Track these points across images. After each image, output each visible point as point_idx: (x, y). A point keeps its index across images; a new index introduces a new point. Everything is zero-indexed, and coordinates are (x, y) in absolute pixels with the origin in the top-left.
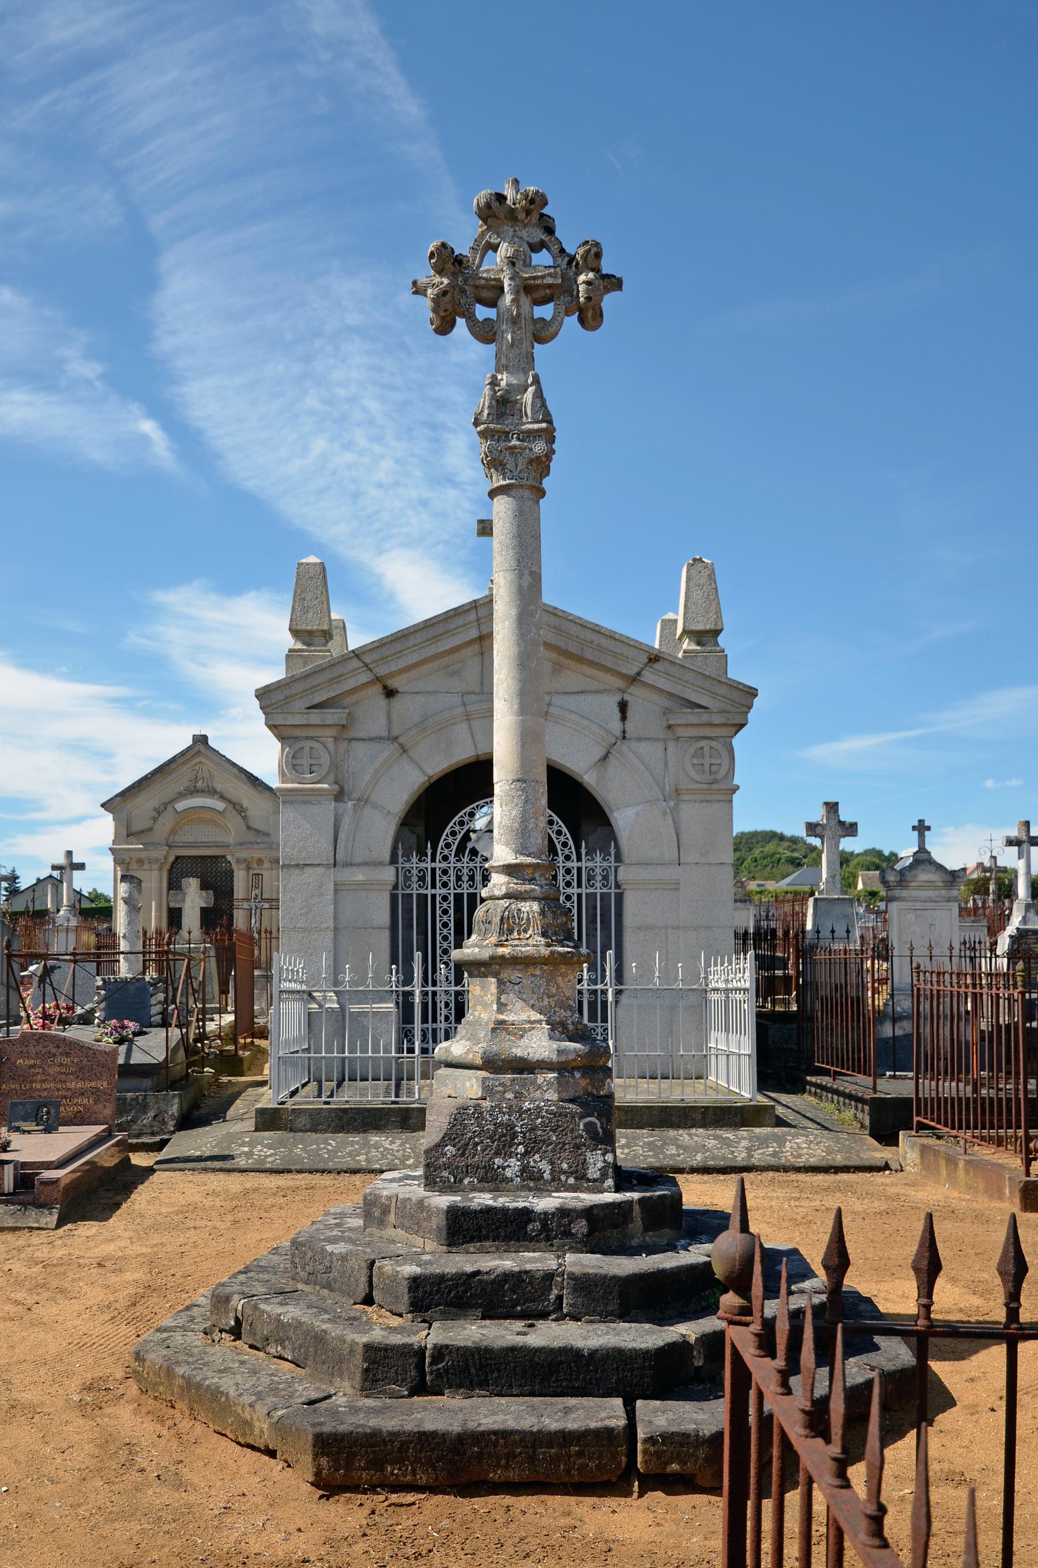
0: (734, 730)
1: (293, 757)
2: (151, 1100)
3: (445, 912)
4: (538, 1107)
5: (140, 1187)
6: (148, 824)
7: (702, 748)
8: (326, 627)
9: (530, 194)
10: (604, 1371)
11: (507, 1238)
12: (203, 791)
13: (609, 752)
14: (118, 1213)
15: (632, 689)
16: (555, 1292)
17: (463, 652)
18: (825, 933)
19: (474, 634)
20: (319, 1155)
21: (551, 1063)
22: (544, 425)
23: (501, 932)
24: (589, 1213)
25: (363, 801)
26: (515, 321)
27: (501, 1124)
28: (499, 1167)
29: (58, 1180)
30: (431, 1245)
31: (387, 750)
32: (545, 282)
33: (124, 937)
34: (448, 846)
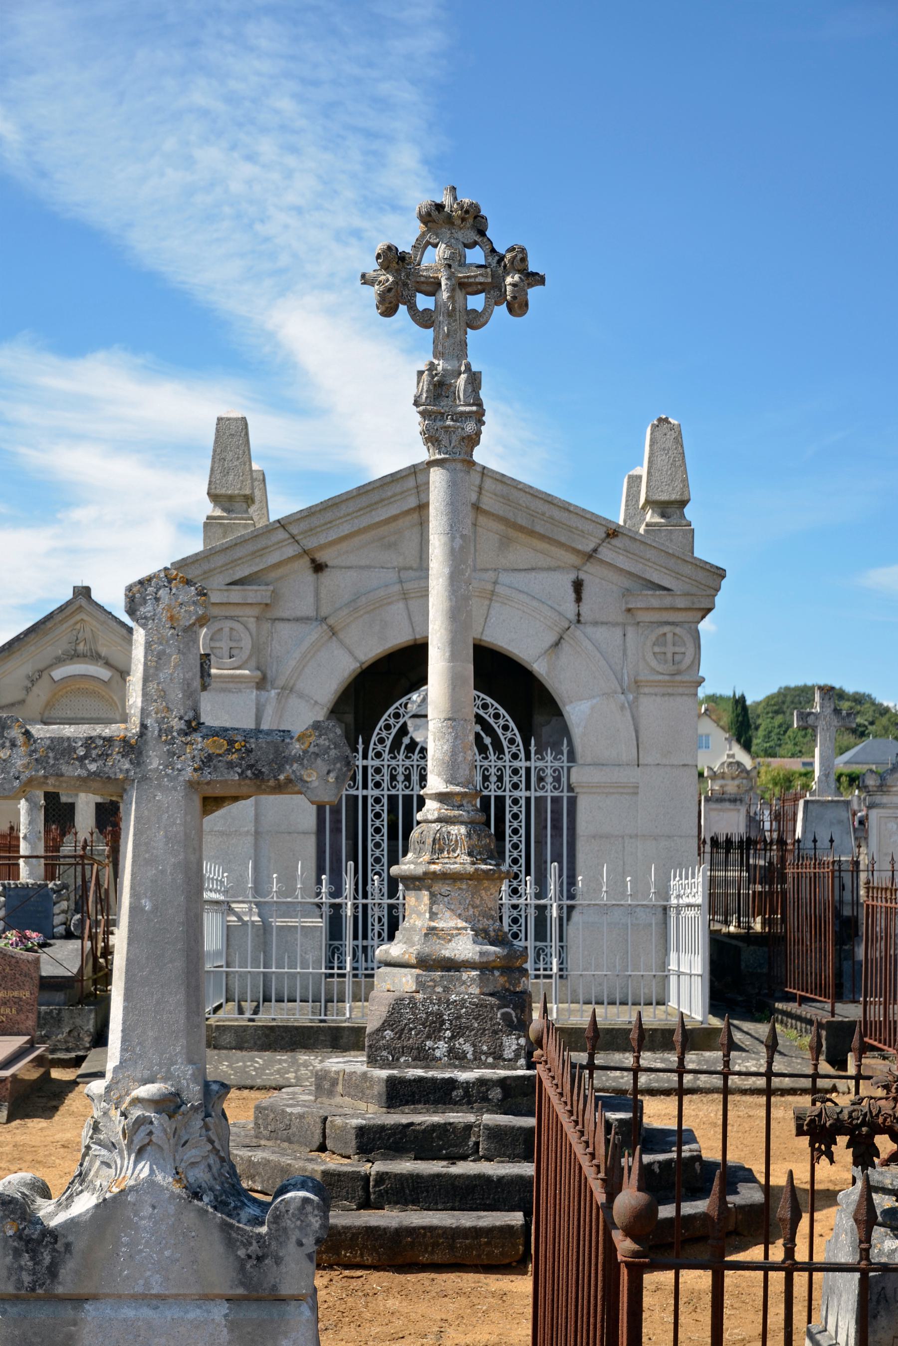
0: (700, 614)
1: (211, 639)
2: (65, 1014)
3: (378, 816)
4: (463, 999)
5: (71, 1095)
6: (19, 695)
7: (665, 634)
8: (248, 492)
9: (465, 205)
10: (509, 1192)
11: (436, 1102)
12: (85, 656)
13: (561, 638)
14: (59, 1113)
15: (589, 567)
16: (473, 1139)
17: (400, 522)
18: (823, 842)
19: (412, 502)
20: (246, 1072)
21: (474, 963)
22: (474, 408)
23: (433, 852)
24: (503, 1082)
25: (288, 690)
26: (450, 314)
27: (432, 1013)
28: (429, 1049)
29: (7, 1078)
30: (373, 1108)
31: (315, 633)
32: (477, 280)
33: (25, 838)
34: (381, 741)
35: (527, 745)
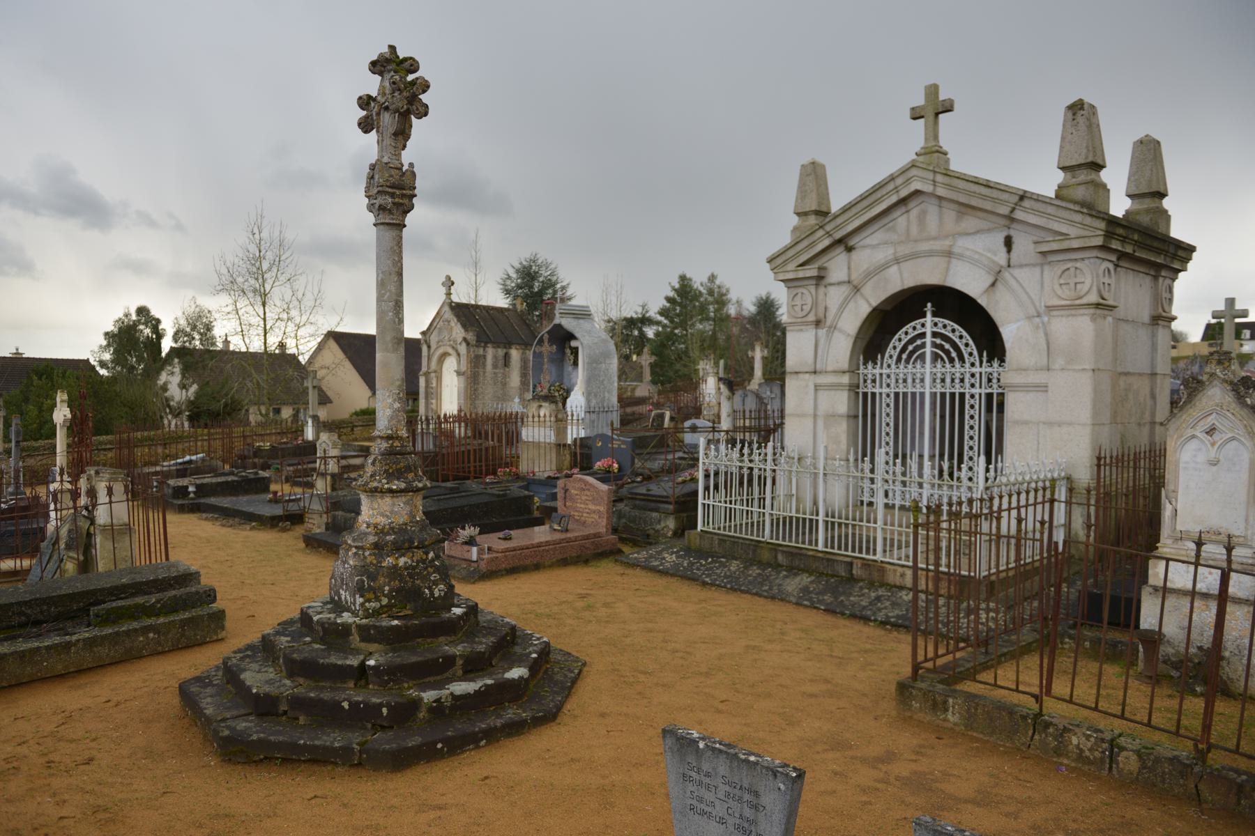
35: (981, 356)
